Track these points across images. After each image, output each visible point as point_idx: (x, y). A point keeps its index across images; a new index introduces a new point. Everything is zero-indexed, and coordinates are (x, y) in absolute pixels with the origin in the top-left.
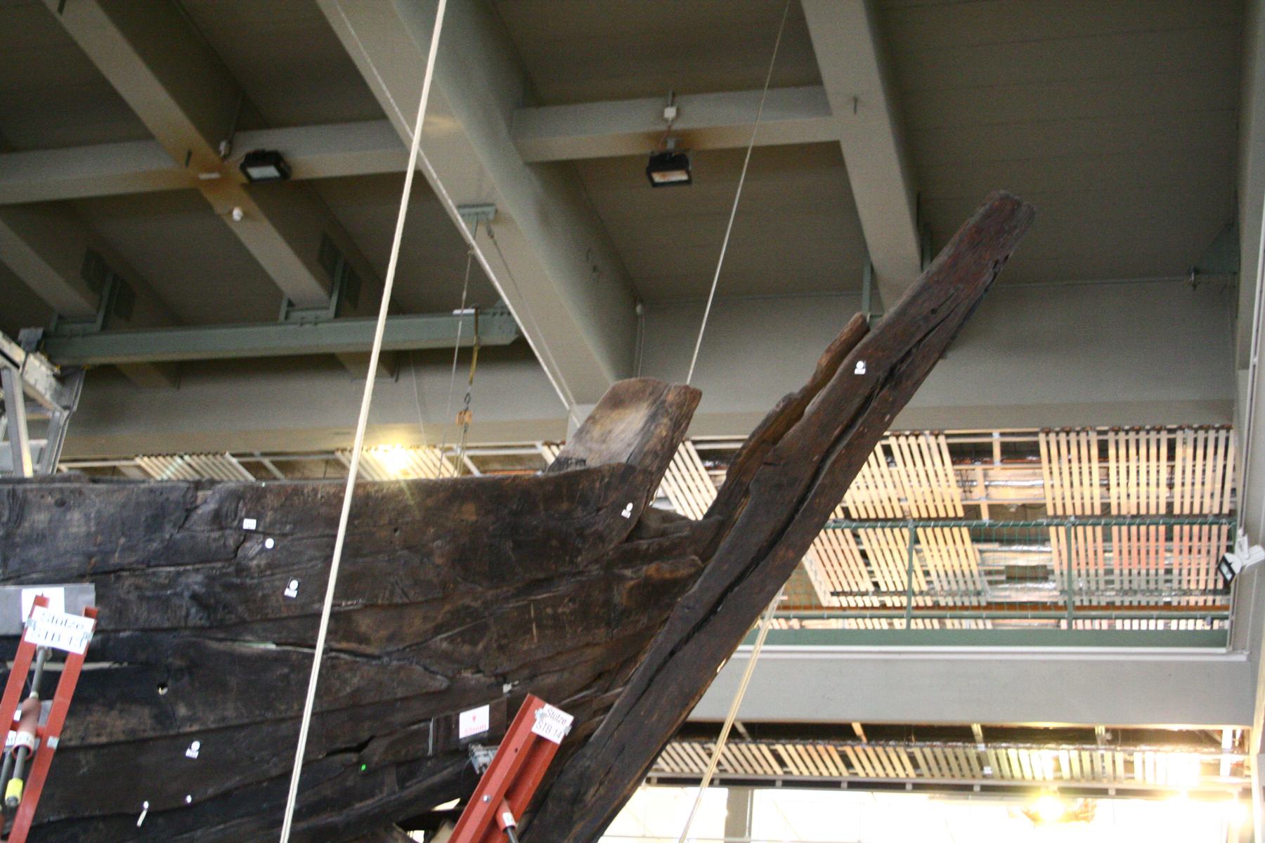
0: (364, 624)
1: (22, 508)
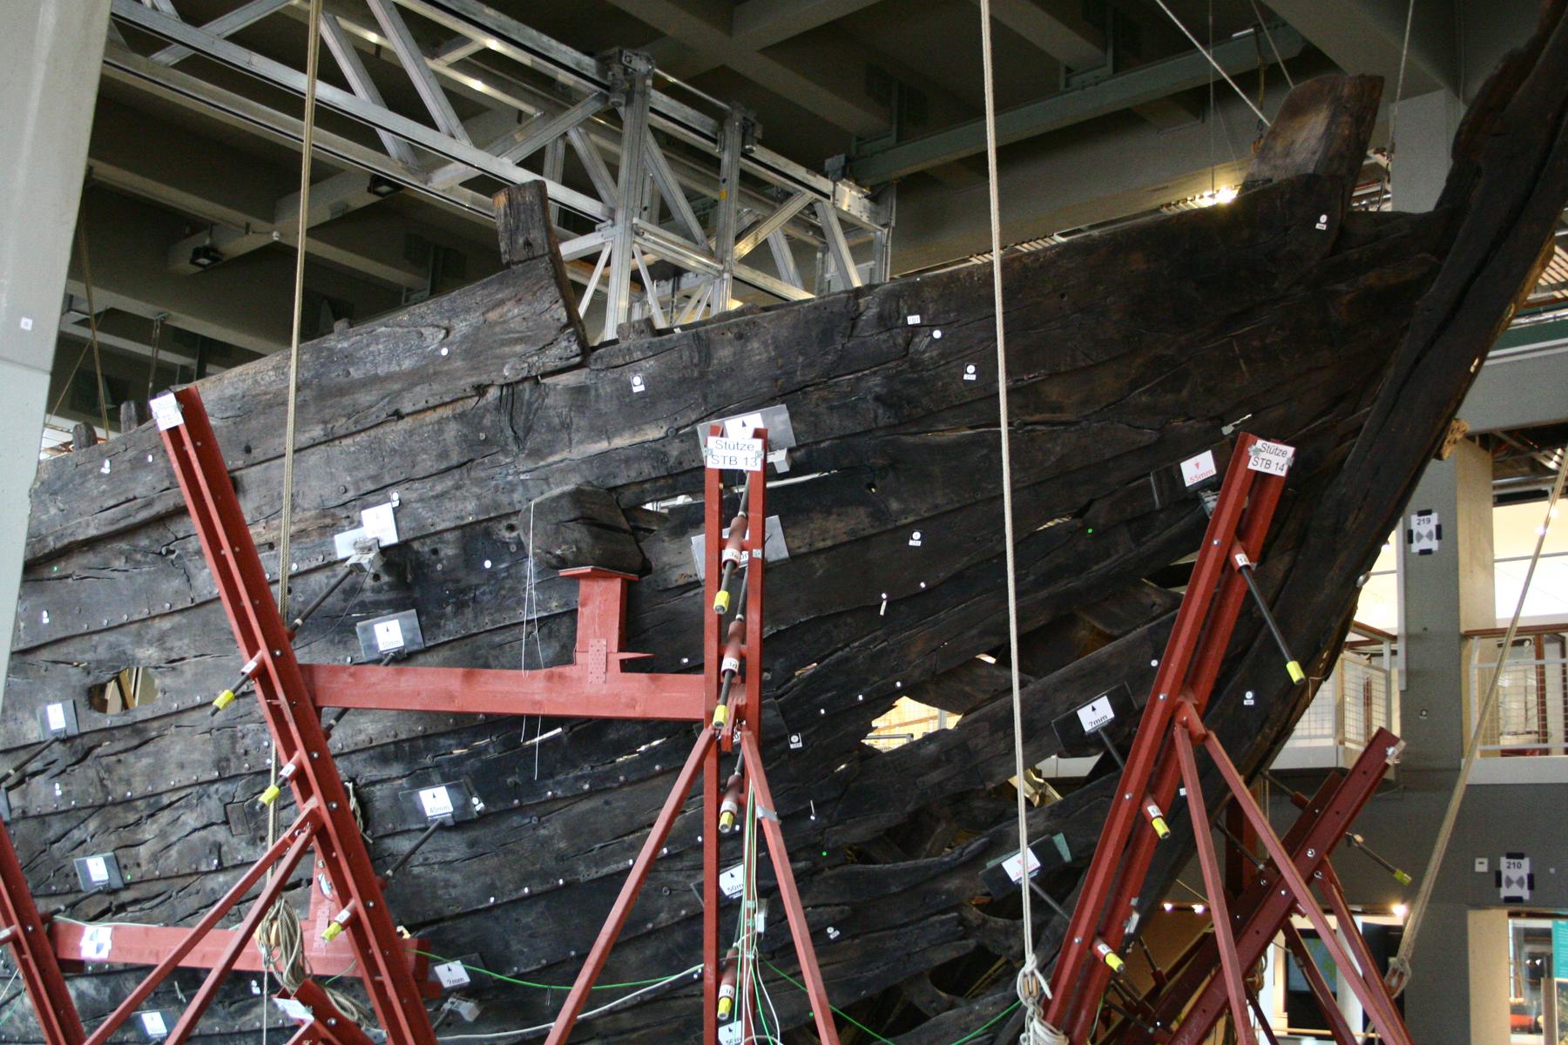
0: (1053, 392)
1: (708, 347)
